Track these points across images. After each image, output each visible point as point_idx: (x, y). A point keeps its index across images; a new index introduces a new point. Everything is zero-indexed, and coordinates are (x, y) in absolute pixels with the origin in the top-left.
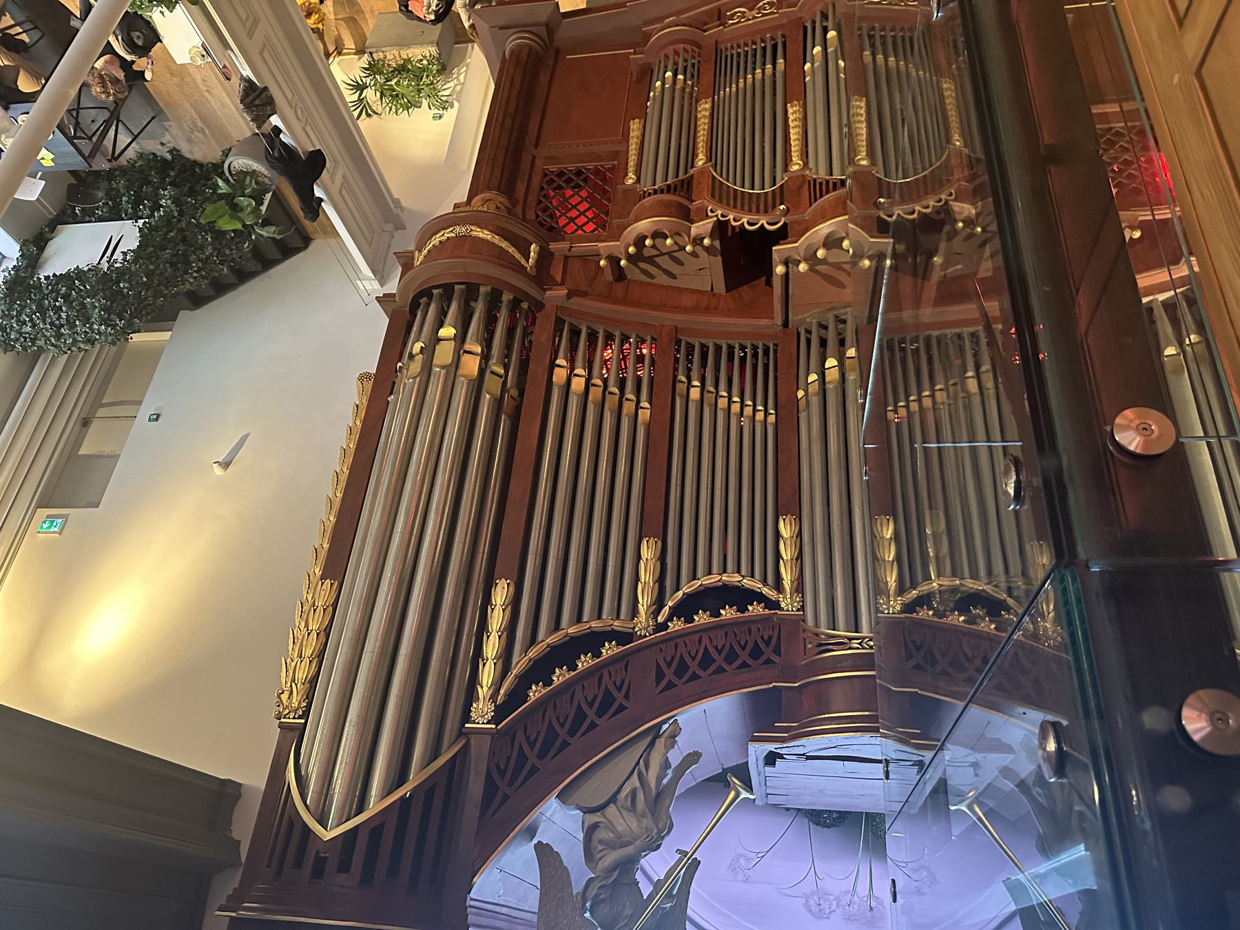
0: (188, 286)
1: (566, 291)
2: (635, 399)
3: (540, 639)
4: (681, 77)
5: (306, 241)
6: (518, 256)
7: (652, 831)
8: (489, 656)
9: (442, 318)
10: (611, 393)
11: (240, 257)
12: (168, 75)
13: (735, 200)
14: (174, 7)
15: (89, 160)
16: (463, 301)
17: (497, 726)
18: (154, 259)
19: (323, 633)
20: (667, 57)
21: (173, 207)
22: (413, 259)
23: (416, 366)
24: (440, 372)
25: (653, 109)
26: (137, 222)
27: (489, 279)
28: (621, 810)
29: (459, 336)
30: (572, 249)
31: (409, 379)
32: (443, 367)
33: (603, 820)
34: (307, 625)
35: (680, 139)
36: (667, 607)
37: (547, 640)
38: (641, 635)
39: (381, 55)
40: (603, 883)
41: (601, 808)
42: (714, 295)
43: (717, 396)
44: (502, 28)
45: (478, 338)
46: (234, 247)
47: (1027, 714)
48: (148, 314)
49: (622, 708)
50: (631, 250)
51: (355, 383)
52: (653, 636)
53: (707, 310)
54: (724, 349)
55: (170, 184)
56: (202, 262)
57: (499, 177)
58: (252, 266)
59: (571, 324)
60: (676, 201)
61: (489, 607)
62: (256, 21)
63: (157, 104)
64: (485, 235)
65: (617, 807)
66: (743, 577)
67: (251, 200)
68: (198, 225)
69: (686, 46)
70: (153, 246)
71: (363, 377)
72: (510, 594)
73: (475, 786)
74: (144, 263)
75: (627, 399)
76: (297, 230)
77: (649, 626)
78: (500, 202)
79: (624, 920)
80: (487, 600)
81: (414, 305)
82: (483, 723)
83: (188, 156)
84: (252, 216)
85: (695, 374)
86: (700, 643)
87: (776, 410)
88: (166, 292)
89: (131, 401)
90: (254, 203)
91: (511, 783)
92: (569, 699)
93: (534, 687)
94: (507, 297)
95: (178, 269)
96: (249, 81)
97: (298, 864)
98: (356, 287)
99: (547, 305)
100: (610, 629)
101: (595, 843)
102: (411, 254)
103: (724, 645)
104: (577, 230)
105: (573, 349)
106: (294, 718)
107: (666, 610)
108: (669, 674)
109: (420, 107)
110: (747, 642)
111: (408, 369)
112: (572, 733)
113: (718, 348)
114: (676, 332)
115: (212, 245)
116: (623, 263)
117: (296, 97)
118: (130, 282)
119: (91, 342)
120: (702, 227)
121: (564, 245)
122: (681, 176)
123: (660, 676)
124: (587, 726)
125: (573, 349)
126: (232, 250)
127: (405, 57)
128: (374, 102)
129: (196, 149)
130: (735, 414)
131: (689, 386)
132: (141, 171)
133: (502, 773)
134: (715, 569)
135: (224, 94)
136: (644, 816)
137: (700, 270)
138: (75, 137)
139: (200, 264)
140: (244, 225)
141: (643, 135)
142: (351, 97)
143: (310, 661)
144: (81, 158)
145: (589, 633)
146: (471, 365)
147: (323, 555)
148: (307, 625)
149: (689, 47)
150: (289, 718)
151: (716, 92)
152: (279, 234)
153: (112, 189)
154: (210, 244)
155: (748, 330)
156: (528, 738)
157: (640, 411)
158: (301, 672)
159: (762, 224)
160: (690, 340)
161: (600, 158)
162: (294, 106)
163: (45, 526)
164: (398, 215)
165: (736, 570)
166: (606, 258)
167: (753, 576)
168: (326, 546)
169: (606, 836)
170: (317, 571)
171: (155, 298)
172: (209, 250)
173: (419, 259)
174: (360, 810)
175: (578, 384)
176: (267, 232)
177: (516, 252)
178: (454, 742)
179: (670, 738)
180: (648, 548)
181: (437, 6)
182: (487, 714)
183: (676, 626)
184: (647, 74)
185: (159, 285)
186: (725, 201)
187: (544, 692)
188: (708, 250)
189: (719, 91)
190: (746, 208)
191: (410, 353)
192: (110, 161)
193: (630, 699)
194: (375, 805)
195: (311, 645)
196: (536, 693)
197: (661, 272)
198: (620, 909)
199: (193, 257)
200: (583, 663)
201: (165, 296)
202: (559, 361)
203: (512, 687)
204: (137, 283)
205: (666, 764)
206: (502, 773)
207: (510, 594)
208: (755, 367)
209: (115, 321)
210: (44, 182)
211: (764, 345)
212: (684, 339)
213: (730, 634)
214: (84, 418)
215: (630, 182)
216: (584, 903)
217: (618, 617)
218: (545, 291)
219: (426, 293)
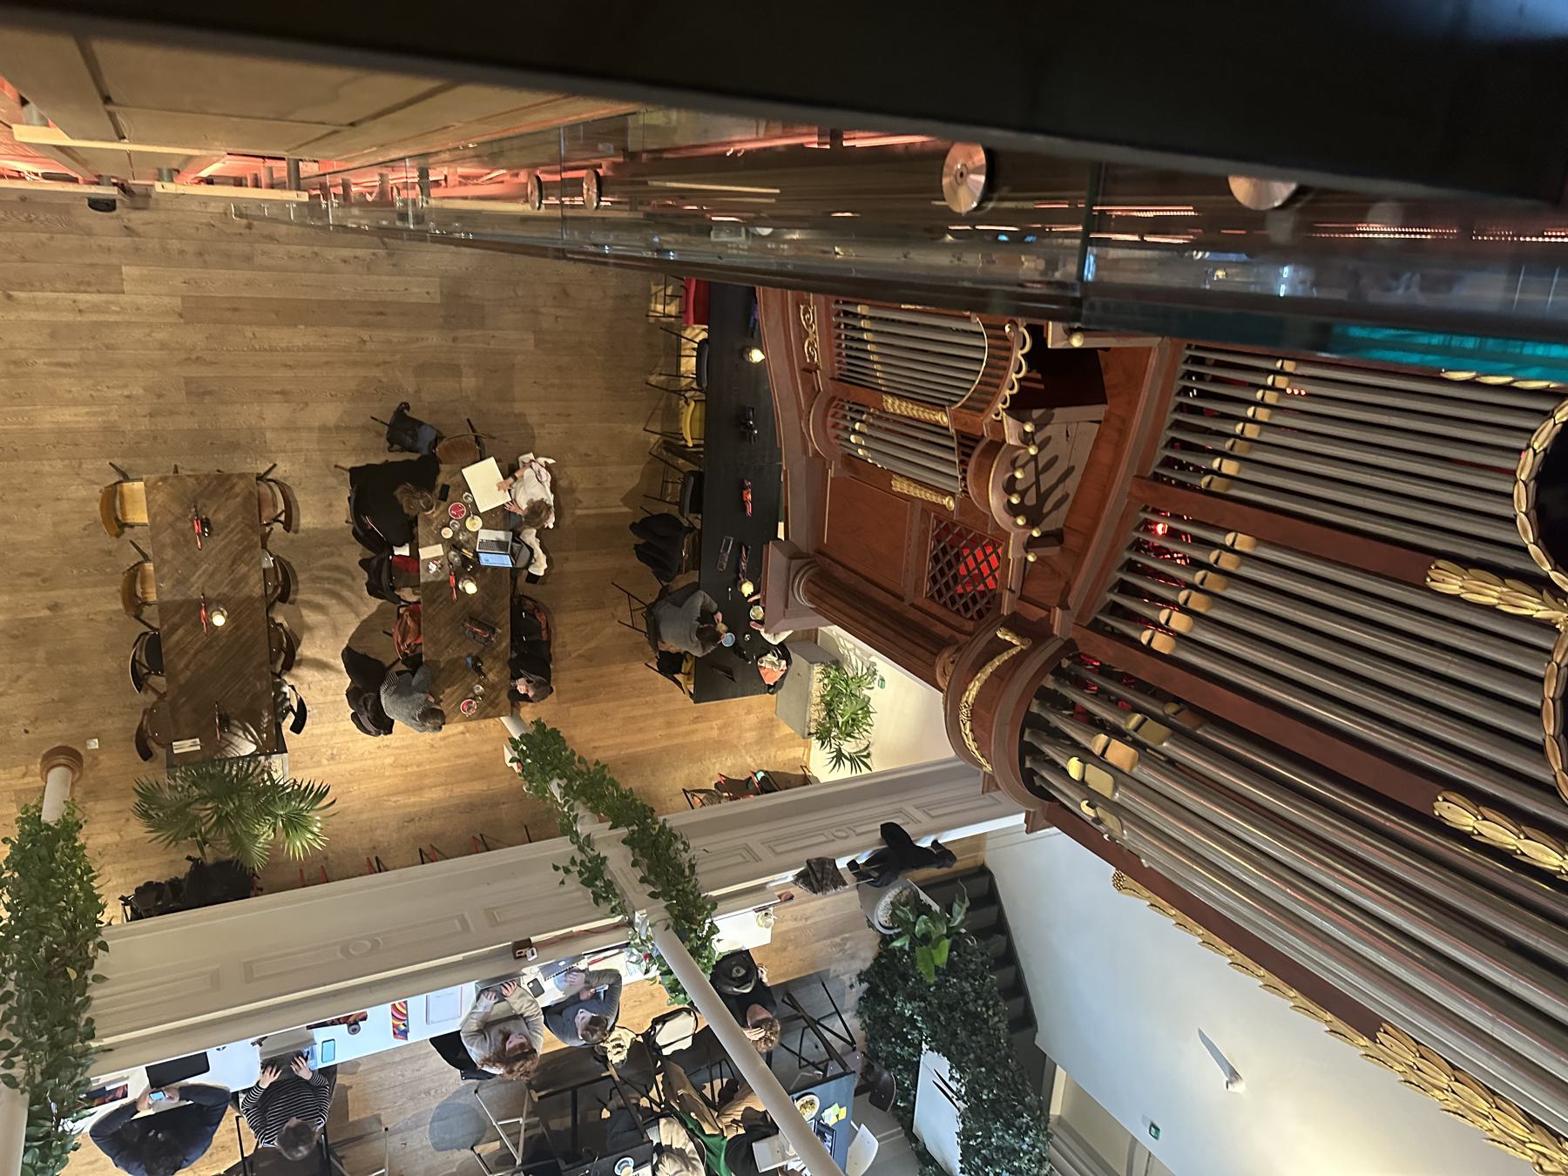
0: (1002, 1026)
1: (1058, 610)
4: (857, 426)
5: (983, 872)
6: (1005, 656)
8: (1557, 863)
10: (1202, 582)
11: (982, 954)
12: (785, 954)
13: (990, 385)
14: (716, 927)
15: (848, 1071)
19: (1457, 1073)
20: (837, 437)
21: (915, 1004)
25: (885, 463)
34: (1441, 1089)
35: (917, 438)
36: (1550, 573)
39: (813, 724)
42: (1106, 420)
43: (1241, 437)
44: (786, 607)
46: (969, 957)
48: (1024, 1084)
50: (1020, 521)
53: (1123, 432)
55: (892, 996)
57: (923, 651)
59: (1102, 612)
60: (979, 456)
61: (1475, 838)
62: (747, 848)
63: (811, 975)
66: (1529, 446)
67: (920, 919)
68: (938, 986)
69: (830, 414)
71: (1117, 883)
72: (1461, 802)
75: (1216, 561)
78: (949, 657)
80: (1463, 837)
81: (1042, 793)
83: (868, 965)
84: (937, 924)
85: (1202, 462)
87: (1278, 359)
94: (1050, 683)
95: (980, 1029)
96: (799, 877)
99: (1071, 636)
104: (994, 577)
109: (869, 699)
113: (1178, 425)
114: (1143, 478)
115: (961, 980)
116: (1035, 533)
117: (826, 832)
119: (1041, 1161)
120: (1011, 431)
121: (1007, 596)
122: (954, 445)
126: (971, 961)
127: (819, 700)
128: (857, 746)
129: (862, 955)
131: (1218, 473)
132: (875, 1020)
135: (812, 904)
137: (1067, 435)
138: (825, 1072)
141: (909, 478)
142: (845, 772)
144: (843, 1078)
146: (1120, 753)
148: (1441, 1089)
149: (832, 411)
151: (878, 387)
152: (964, 902)
153: (886, 1059)
155: (1160, 382)
158: (1511, 1127)
159: (1022, 355)
160: (1158, 460)
161: (925, 532)
162: (833, 838)
165: (1517, 456)
166: (1027, 552)
167: (1532, 431)
168: (1329, 1017)
175: (1180, 622)
180: (1443, 581)
181: (774, 655)
184: (850, 461)
185: (994, 1058)
186: (989, 398)
188: (1039, 426)
189: (878, 384)
190: (1001, 373)
192: (854, 1049)
197: (1061, 486)
199: (971, 1006)
201: (1008, 1056)
202: (1144, 639)
208: (1217, 380)
210: (863, 1125)
211: (1186, 362)
212: (1153, 468)
215: (952, 504)
217: (1549, 652)
218: (1053, 635)
219: (1028, 777)
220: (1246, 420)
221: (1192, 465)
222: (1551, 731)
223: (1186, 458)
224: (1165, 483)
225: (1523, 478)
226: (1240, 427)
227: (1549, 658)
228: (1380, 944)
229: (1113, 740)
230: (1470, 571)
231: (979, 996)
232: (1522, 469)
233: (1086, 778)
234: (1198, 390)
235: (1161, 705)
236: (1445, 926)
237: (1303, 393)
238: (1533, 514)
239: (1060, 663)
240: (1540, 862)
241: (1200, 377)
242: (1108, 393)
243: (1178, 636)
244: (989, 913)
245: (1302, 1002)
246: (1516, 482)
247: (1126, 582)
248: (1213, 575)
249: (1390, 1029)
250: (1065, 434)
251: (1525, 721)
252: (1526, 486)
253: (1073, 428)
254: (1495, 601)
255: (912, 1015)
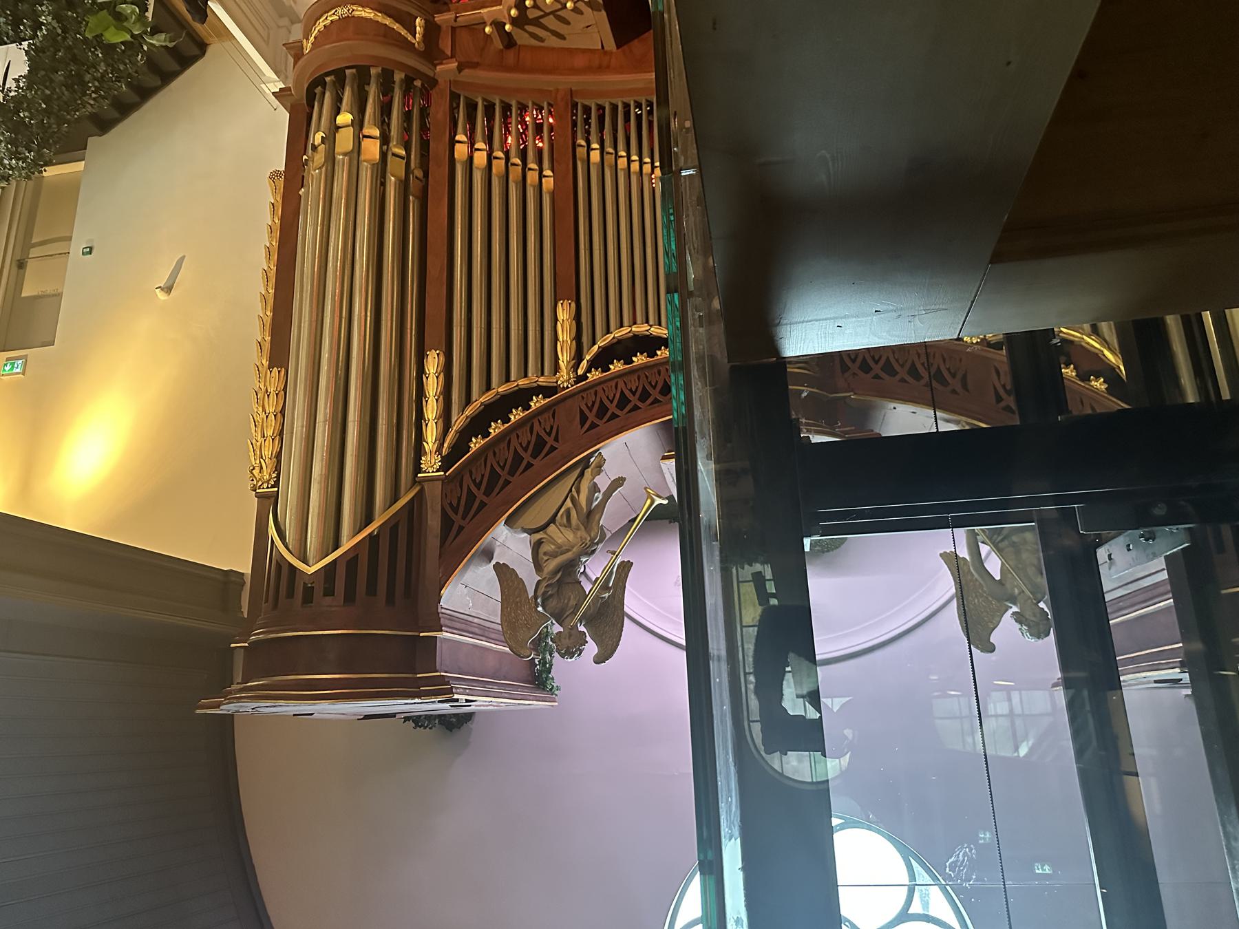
0: (89, 109)
1: (456, 64)
2: (537, 168)
3: (474, 399)
5: (202, 47)
6: (403, 32)
7: (586, 539)
8: (430, 417)
9: (339, 104)
10: (513, 164)
16: (355, 87)
17: (445, 473)
18: (48, 84)
19: (279, 415)
21: (55, 24)
22: (303, 48)
23: (320, 158)
24: (343, 159)
26: (21, 44)
27: (378, 60)
28: (560, 527)
29: (356, 122)
30: (458, 19)
31: (315, 170)
32: (345, 154)
33: (545, 536)
34: (264, 410)
37: (480, 400)
38: (563, 387)
40: (549, 582)
41: (544, 528)
42: (606, 53)
43: (617, 157)
45: (375, 122)
46: (128, 61)
47: (897, 409)
48: (55, 143)
49: (553, 449)
50: (513, 12)
51: (267, 181)
52: (575, 387)
53: (601, 69)
54: (620, 108)
56: (98, 81)
58: (151, 80)
61: (424, 376)
64: (367, 13)
65: (556, 525)
66: (651, 326)
67: (134, 6)
70: (44, 70)
71: (274, 175)
72: (441, 362)
73: (433, 522)
74: (39, 89)
75: (530, 169)
76: (188, 34)
77: (570, 379)
79: (570, 610)
80: (421, 370)
81: (311, 98)
82: (433, 472)
85: (594, 137)
86: (616, 388)
88: (69, 117)
89: (60, 238)
90: (138, 10)
91: (464, 518)
92: (506, 448)
93: (474, 439)
94: (398, 76)
97: (291, 594)
98: (262, 92)
99: (439, 80)
100: (535, 385)
101: (541, 555)
102: (299, 44)
103: (637, 387)
105: (471, 119)
106: (268, 488)
107: (584, 364)
108: (591, 417)
110: (657, 382)
111: (313, 161)
112: (512, 473)
113: (614, 108)
114: (571, 97)
116: (508, 27)
118: (28, 109)
123: (583, 419)
124: (524, 465)
125: (471, 119)
130: (635, 173)
131: (589, 149)
133: (456, 511)
134: (626, 321)
136: (578, 529)
137: (587, 27)
139: (97, 84)
140: (133, 36)
143: (273, 439)
145: (517, 390)
146: (372, 149)
147: (267, 347)
148: (264, 410)
150: (263, 488)
152: (170, 42)
154: (101, 61)
156: (474, 481)
157: (544, 180)
158: (267, 449)
160: (587, 103)
163: (7, 368)
164: (291, 7)
165: (644, 321)
166: (491, 25)
168: (268, 338)
169: (549, 548)
170: (264, 362)
171: (59, 125)
172: (102, 68)
173: (308, 46)
174: (336, 547)
175: (480, 159)
176: (158, 41)
177: (402, 28)
178: (411, 488)
179: (597, 467)
182: (435, 464)
183: (595, 375)
185: (59, 110)
187: (483, 442)
191: (313, 145)
193: (560, 442)
194: (347, 544)
195: (271, 425)
196: (476, 444)
197: (549, 34)
198: (566, 601)
199: (88, 77)
200: (515, 416)
201: (68, 122)
203: (454, 441)
204: (37, 110)
205: (595, 488)
206: (456, 511)
207: (441, 362)
209: (25, 154)
212: (580, 101)
213: (643, 376)
214: (19, 261)
216: (536, 600)
217: (542, 374)
218: (435, 66)
219: (319, 82)
220: (629, 157)
221: (590, 127)
222: (500, 390)
223: (593, 121)
224: (572, 112)
225: (633, 329)
226: (624, 154)
227: (539, 374)
228: (334, 352)
229: (378, 141)
230: (574, 321)
231: (102, 79)
232: (638, 327)
233: (340, 130)
234: (641, 114)
235: (417, 165)
236: (365, 379)
237: (654, 185)
238: (615, 340)
239: (415, 79)
240: (427, 410)
241: (650, 113)
242: (625, 47)
243: (471, 158)
244: (170, 64)
245: (267, 321)
246: (630, 326)
247: (494, 109)
248: (520, 171)
249: (283, 373)
250: (587, 25)
251: (500, 375)
252: (629, 332)
253: (593, 29)
254: (561, 340)
255: (43, 24)
